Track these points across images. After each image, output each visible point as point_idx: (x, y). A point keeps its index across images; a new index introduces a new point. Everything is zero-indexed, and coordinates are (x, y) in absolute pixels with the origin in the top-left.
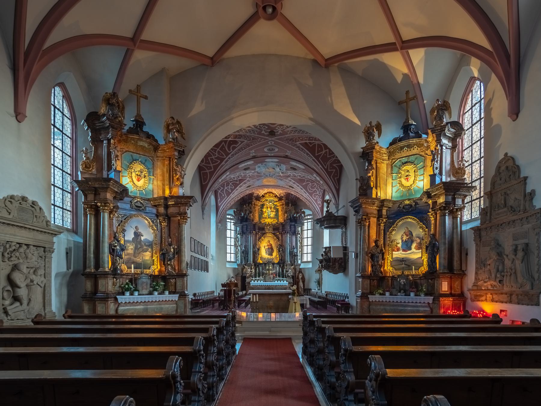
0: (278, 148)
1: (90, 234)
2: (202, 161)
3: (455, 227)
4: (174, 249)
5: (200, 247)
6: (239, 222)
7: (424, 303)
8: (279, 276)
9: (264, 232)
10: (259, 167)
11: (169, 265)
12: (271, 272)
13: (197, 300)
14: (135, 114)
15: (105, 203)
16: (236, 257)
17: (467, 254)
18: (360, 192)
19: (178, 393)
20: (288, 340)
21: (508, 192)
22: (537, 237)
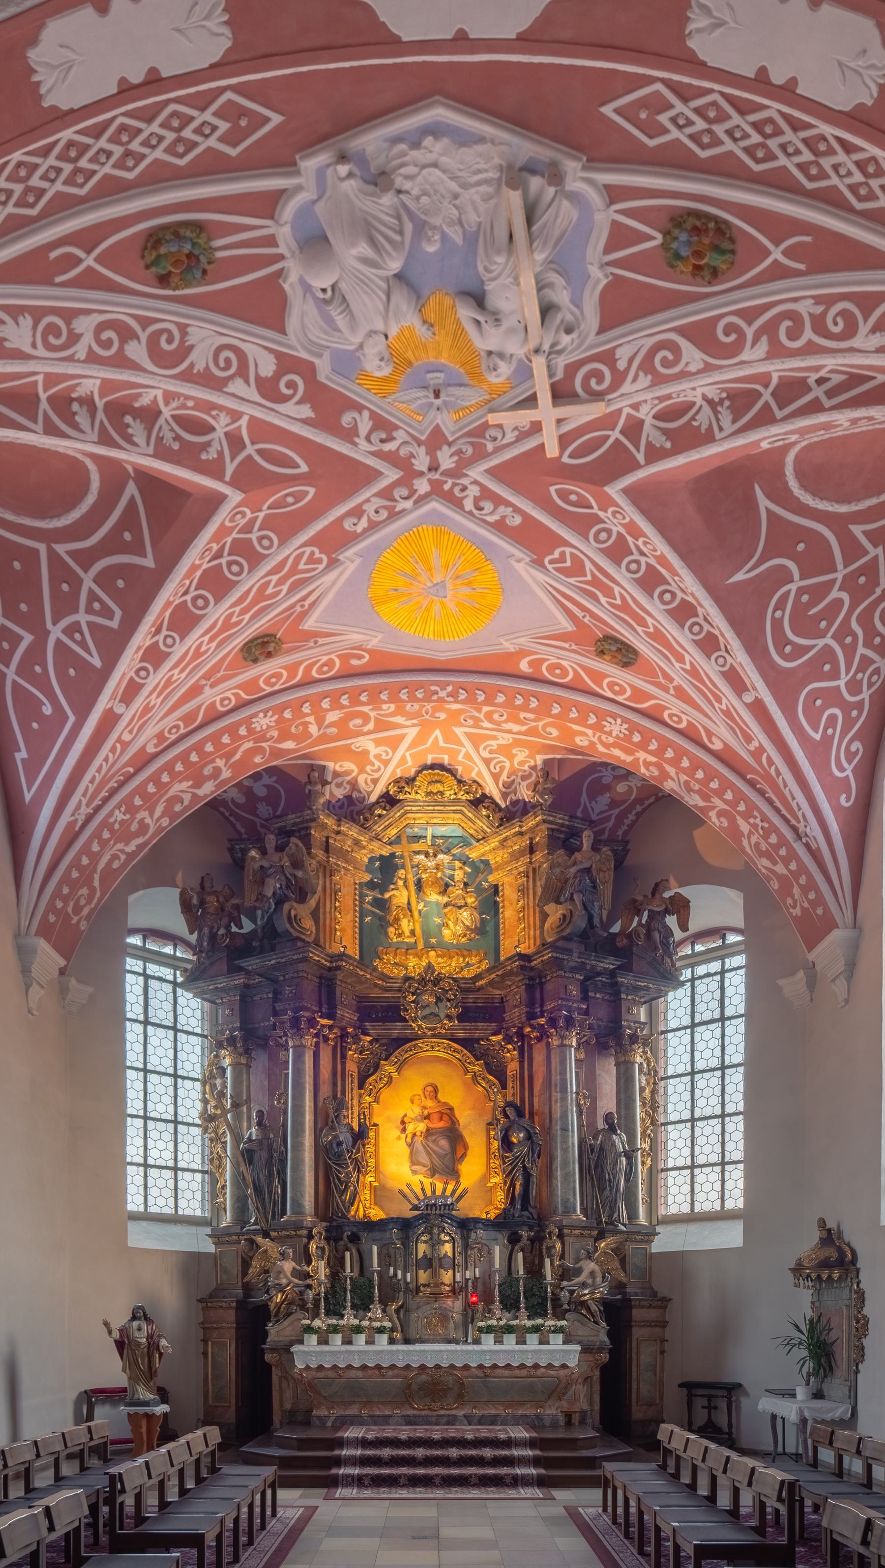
8: (510, 1304)
9: (396, 1030)
12: (447, 1277)
16: (214, 1191)
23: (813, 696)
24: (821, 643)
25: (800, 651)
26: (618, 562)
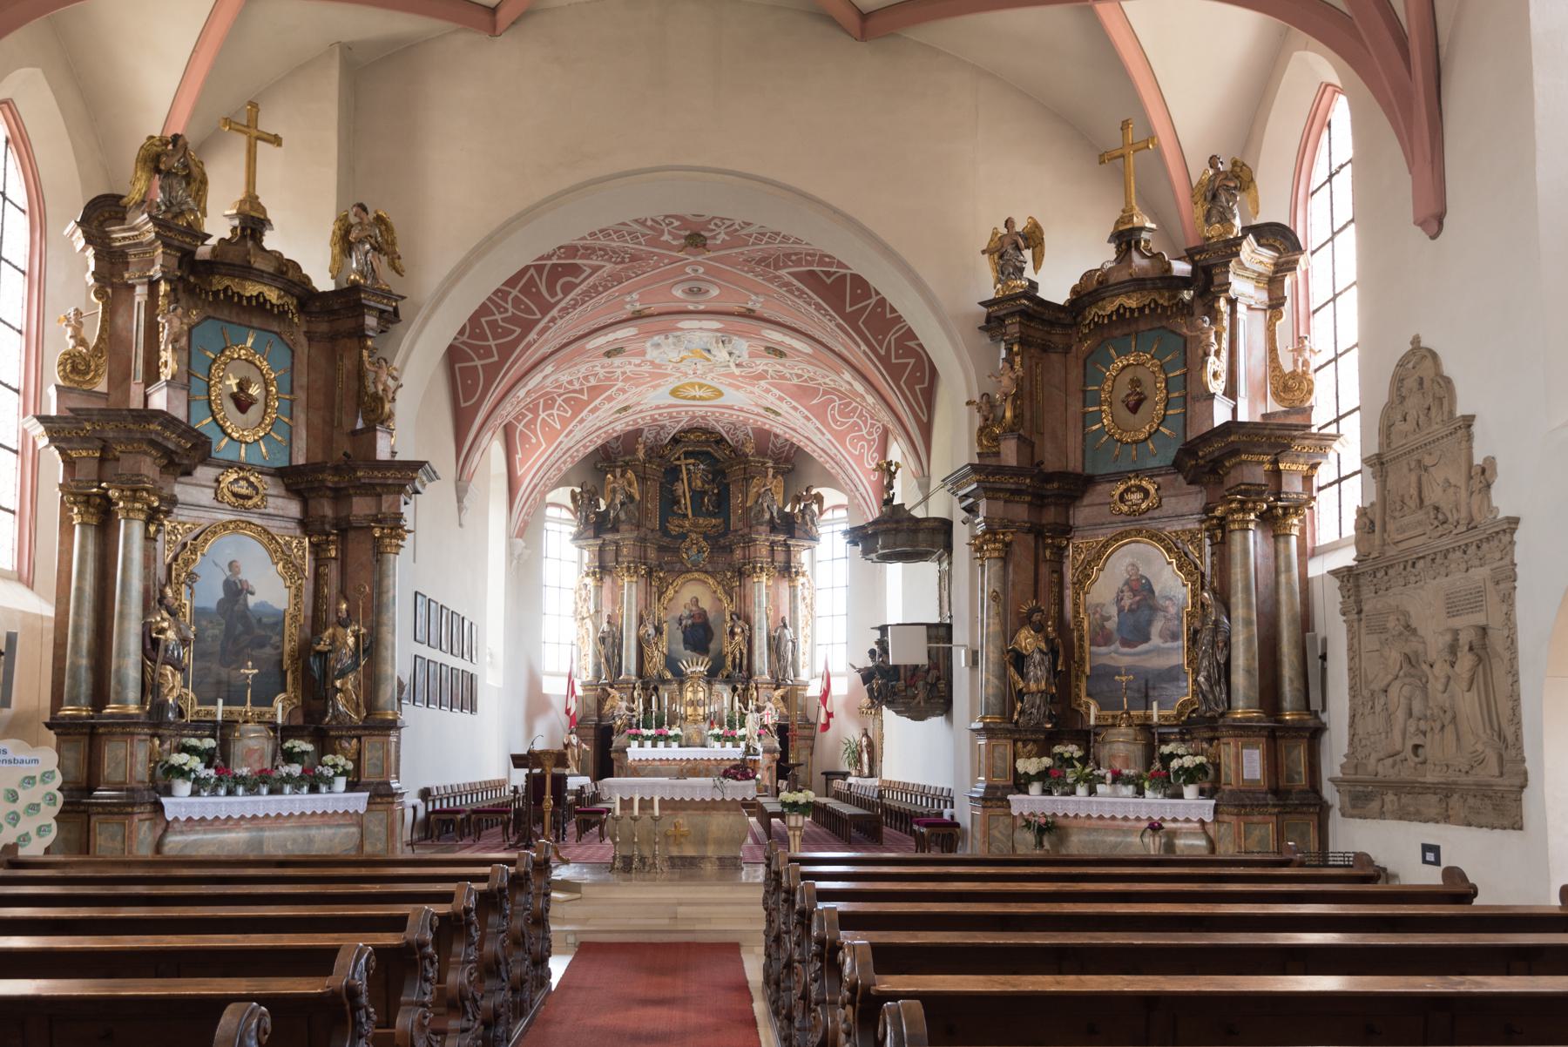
0: (719, 286)
1: (80, 589)
2: (462, 332)
3: (1283, 568)
4: (357, 637)
5: (450, 628)
7: (1188, 820)
10: (658, 345)
11: (340, 690)
13: (441, 811)
14: (240, 194)
15: (135, 491)
17: (1324, 657)
18: (980, 444)
19: (360, 1037)
20: (731, 949)
21: (1427, 461)
22: (1505, 608)
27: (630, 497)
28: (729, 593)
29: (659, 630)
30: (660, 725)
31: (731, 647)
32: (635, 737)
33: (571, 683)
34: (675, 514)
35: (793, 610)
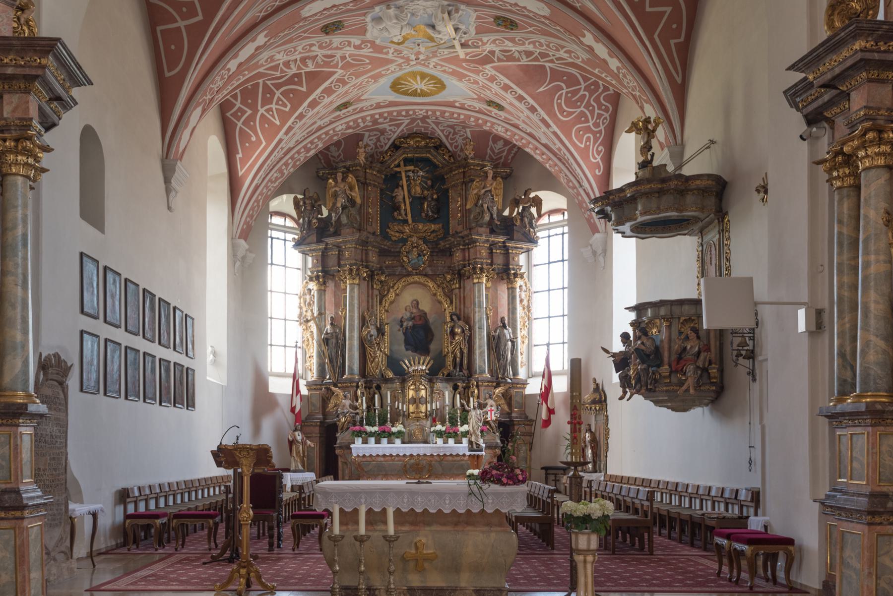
6: (314, 238)
10: (378, 20)
15: (17, 140)
23: (579, 130)
24: (579, 110)
25: (571, 113)
26: (492, 82)
27: (352, 201)
28: (449, 296)
29: (380, 331)
30: (383, 422)
31: (450, 347)
32: (359, 434)
33: (295, 378)
34: (395, 220)
35: (512, 310)
